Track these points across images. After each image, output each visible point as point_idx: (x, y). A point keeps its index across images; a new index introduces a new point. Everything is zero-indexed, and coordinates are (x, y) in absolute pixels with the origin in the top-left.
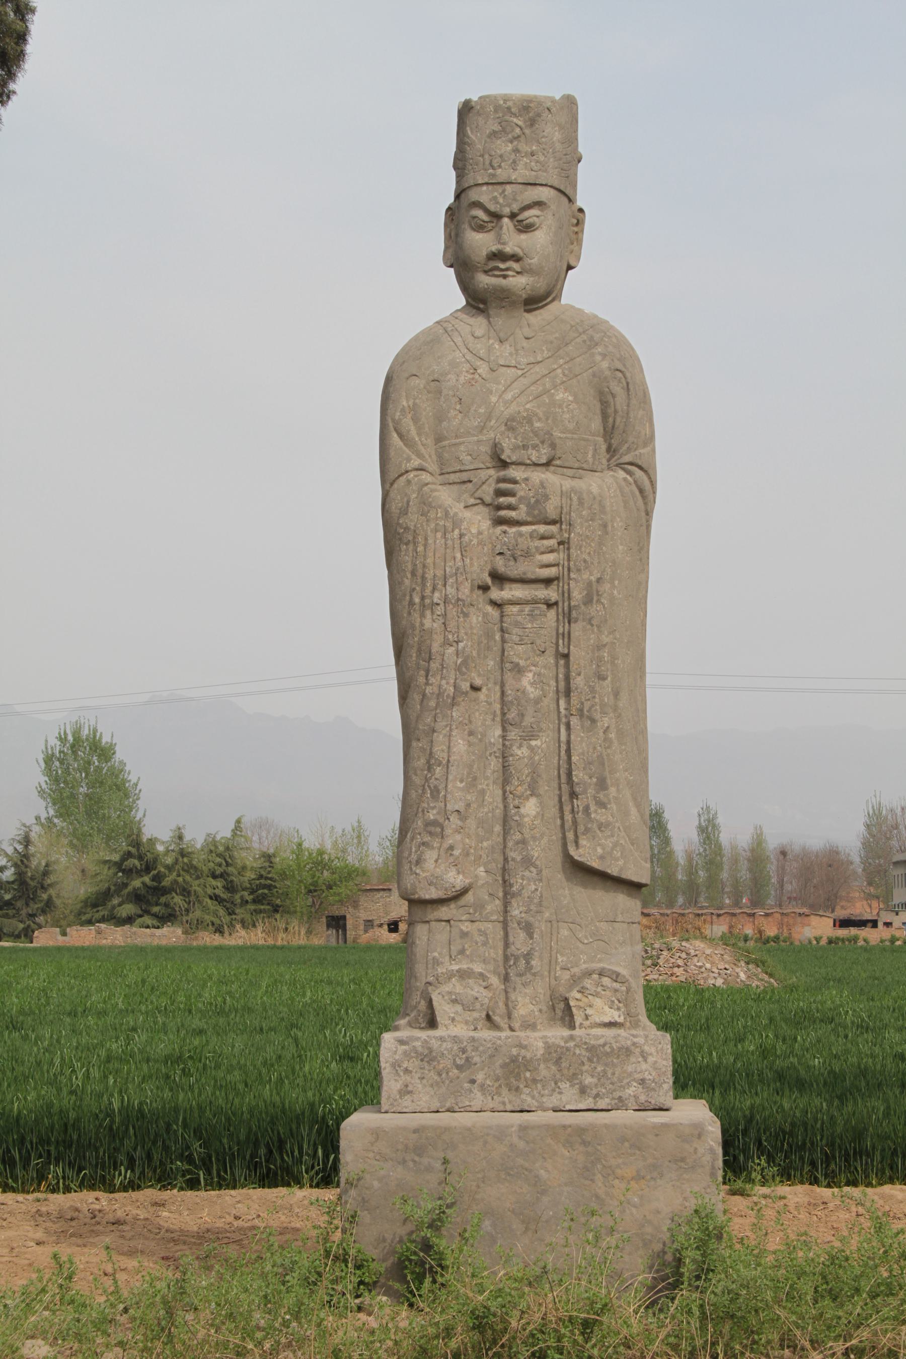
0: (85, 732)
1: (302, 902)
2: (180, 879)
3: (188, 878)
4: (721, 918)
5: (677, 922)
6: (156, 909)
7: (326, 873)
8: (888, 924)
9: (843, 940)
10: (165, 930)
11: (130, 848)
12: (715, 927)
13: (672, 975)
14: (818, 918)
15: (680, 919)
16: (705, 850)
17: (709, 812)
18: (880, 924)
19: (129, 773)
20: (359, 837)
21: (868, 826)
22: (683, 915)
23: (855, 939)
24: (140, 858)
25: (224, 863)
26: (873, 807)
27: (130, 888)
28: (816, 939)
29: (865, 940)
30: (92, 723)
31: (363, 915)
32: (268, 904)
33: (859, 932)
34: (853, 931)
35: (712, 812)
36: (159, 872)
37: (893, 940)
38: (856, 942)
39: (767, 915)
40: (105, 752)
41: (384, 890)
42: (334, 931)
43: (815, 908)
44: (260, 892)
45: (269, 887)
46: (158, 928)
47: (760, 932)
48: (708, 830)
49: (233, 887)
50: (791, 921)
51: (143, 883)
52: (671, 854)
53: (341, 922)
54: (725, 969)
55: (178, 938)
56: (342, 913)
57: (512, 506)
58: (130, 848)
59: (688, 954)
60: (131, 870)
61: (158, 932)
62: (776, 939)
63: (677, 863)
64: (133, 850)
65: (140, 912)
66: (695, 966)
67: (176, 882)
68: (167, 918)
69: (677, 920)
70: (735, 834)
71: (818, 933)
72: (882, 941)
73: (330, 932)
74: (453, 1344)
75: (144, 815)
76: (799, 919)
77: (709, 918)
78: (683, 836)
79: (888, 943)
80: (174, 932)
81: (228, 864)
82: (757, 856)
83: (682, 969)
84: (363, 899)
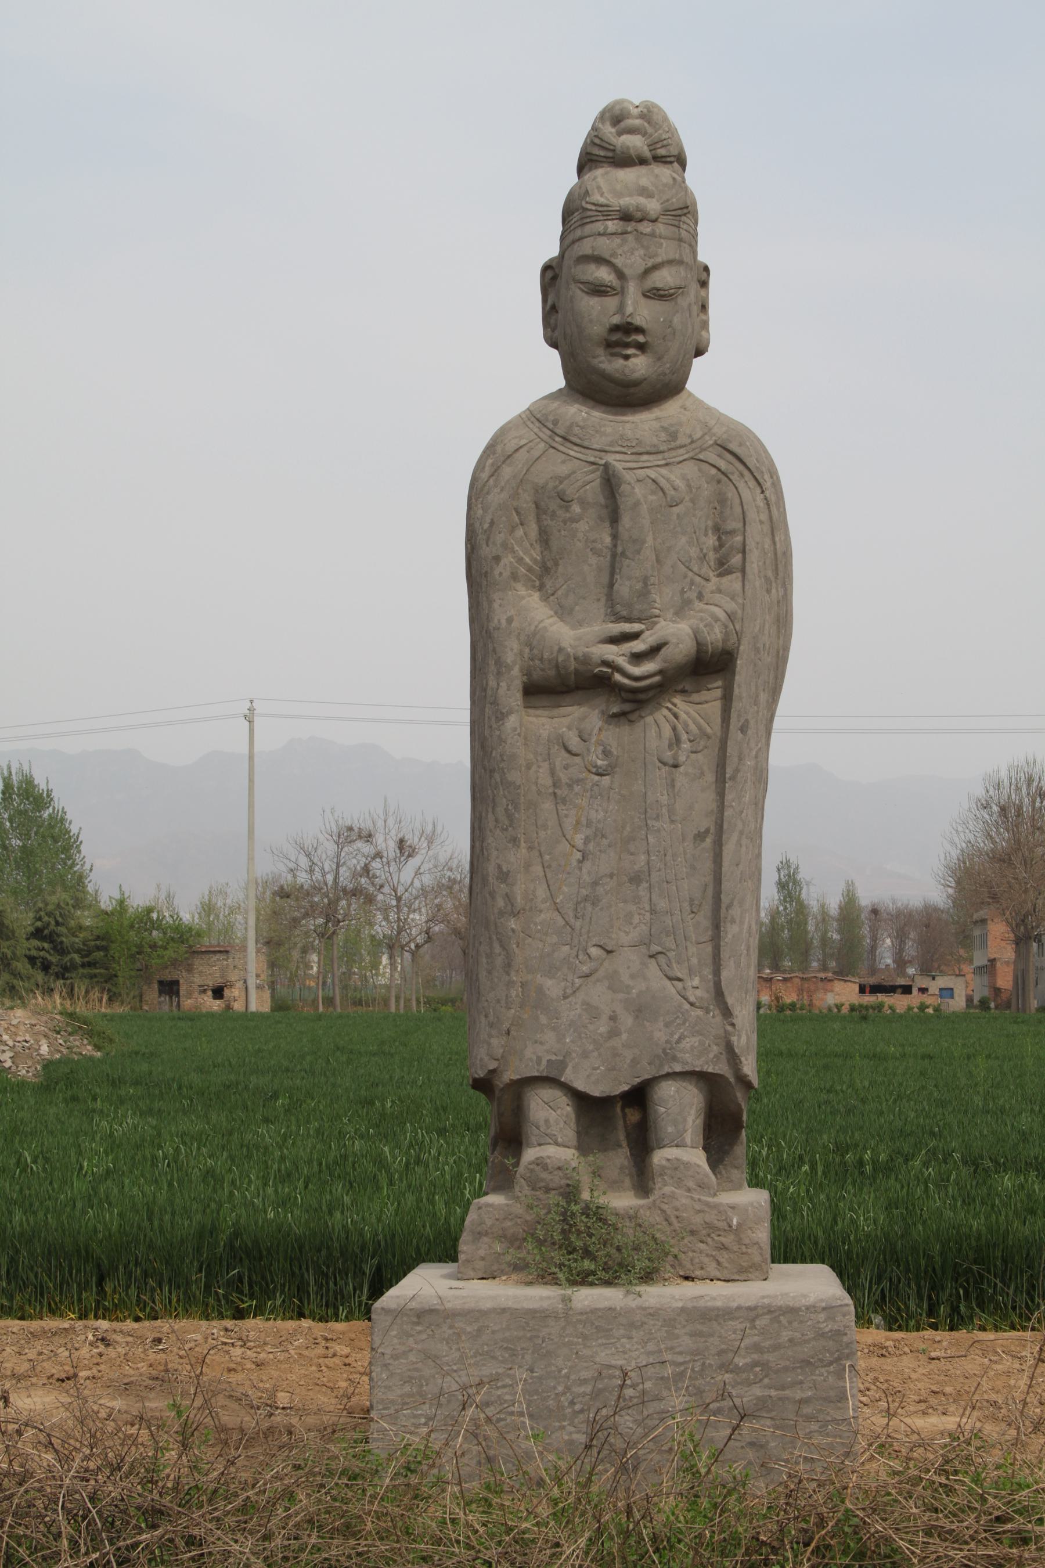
0: (15, 779)
7: (155, 933)
8: (923, 990)
9: (867, 1008)
14: (842, 983)
16: (786, 908)
17: (789, 867)
18: (915, 991)
19: (70, 823)
23: (879, 1007)
25: (53, 923)
28: (837, 1006)
29: (890, 1008)
30: (26, 768)
31: (198, 980)
34: (881, 997)
35: (793, 867)
37: (923, 1007)
38: (879, 1011)
43: (843, 973)
45: (105, 949)
47: (778, 999)
49: (62, 948)
50: (812, 987)
53: (175, 988)
54: (26, 1041)
56: (175, 977)
57: (621, 566)
62: (793, 1006)
71: (838, 1000)
72: (910, 1009)
73: (162, 999)
76: (820, 984)
81: (57, 924)
84: (198, 962)
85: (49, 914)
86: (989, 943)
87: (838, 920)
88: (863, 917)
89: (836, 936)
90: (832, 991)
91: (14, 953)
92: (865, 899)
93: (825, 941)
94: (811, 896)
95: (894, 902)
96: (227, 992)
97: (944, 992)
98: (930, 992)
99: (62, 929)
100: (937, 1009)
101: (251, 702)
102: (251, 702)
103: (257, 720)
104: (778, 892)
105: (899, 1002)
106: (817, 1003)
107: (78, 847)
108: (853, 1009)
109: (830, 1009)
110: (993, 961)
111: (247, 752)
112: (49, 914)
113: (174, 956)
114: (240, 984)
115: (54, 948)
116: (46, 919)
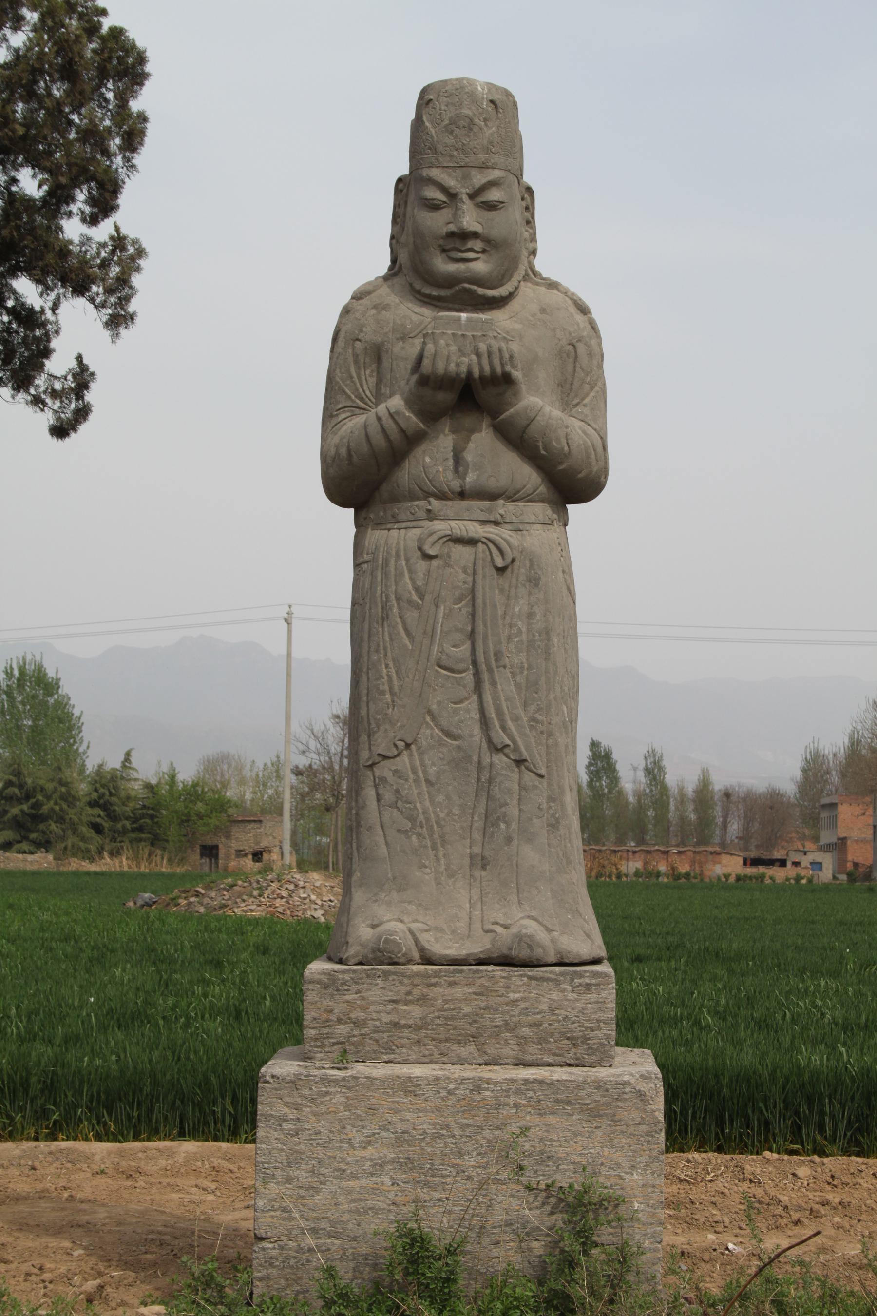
1: (173, 833)
2: (57, 808)
3: (65, 806)
4: (637, 855)
5: (595, 858)
6: (33, 836)
8: (796, 864)
9: (751, 878)
10: (37, 856)
11: (11, 777)
12: (631, 864)
13: (270, 906)
14: (728, 856)
15: (597, 855)
16: (651, 791)
17: (654, 755)
18: (789, 864)
20: (277, 771)
21: (804, 771)
22: (600, 851)
23: (762, 877)
24: (21, 786)
25: (107, 793)
26: (810, 752)
27: (9, 815)
29: (771, 878)
30: (38, 658)
31: (235, 845)
32: (149, 833)
33: (766, 871)
34: (762, 869)
35: (658, 755)
36: (38, 801)
37: (798, 879)
38: (762, 881)
39: (680, 853)
40: (50, 687)
41: (255, 821)
42: (208, 860)
44: (142, 821)
45: (152, 817)
46: (31, 853)
48: (654, 770)
49: (115, 816)
51: (22, 811)
52: (620, 792)
53: (214, 852)
54: (330, 901)
55: (49, 863)
56: (215, 842)
58: (11, 777)
59: (296, 886)
60: (11, 798)
61: (30, 858)
62: (687, 876)
63: (627, 802)
64: (14, 779)
65: (19, 838)
66: (300, 897)
67: (52, 809)
68: (45, 844)
69: (594, 857)
70: (681, 776)
72: (788, 879)
73: (203, 861)
74: (495, 1252)
75: (88, 747)
76: (710, 857)
77: (625, 855)
78: (630, 779)
79: (792, 882)
80: (46, 857)
81: (111, 794)
82: (703, 795)
83: (284, 900)
84: (235, 830)
85: (103, 786)
86: (839, 824)
87: (694, 801)
88: (716, 798)
89: (693, 817)
90: (720, 863)
91: (80, 819)
92: (718, 783)
93: (682, 819)
94: (671, 779)
95: (739, 787)
96: (265, 856)
97: (814, 865)
98: (803, 864)
99: (114, 799)
100: (810, 881)
101: (290, 607)
102: (290, 607)
103: (295, 623)
104: (645, 777)
105: (779, 874)
106: (707, 873)
107: (79, 728)
108: (738, 879)
109: (719, 879)
110: (844, 840)
111: (285, 653)
112: (103, 786)
113: (217, 823)
114: (276, 850)
115: (108, 816)
116: (102, 790)
